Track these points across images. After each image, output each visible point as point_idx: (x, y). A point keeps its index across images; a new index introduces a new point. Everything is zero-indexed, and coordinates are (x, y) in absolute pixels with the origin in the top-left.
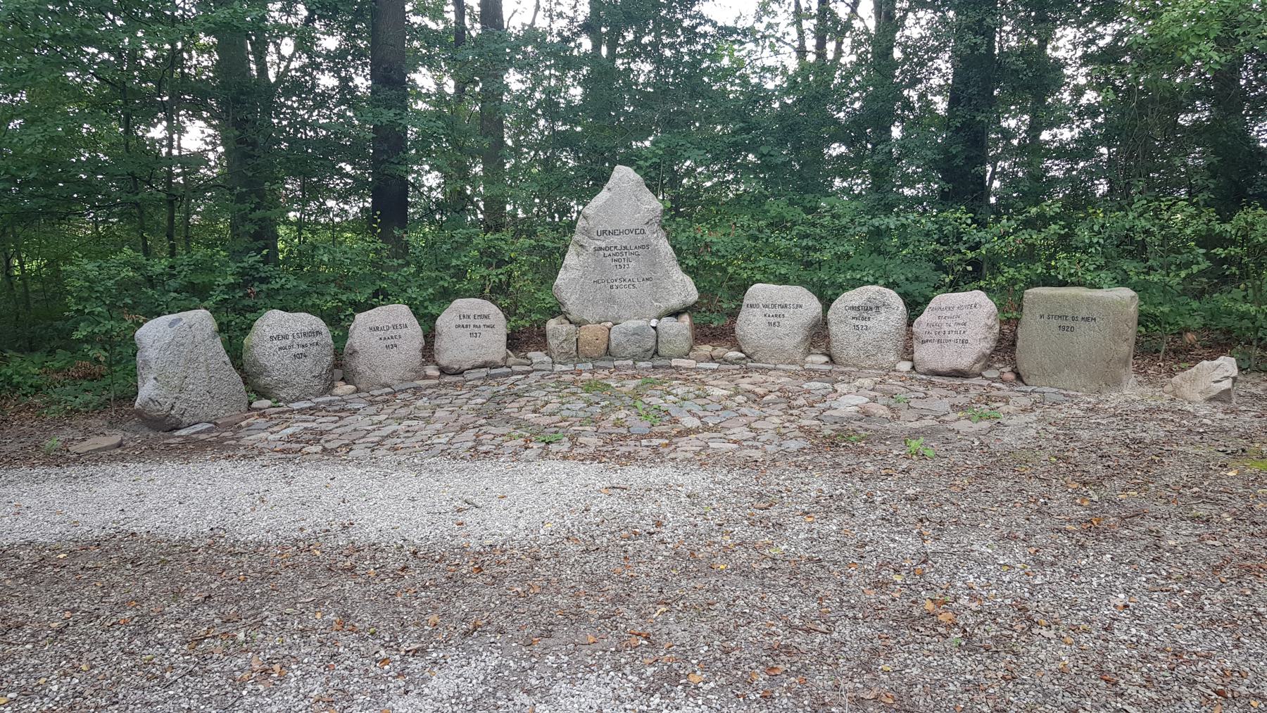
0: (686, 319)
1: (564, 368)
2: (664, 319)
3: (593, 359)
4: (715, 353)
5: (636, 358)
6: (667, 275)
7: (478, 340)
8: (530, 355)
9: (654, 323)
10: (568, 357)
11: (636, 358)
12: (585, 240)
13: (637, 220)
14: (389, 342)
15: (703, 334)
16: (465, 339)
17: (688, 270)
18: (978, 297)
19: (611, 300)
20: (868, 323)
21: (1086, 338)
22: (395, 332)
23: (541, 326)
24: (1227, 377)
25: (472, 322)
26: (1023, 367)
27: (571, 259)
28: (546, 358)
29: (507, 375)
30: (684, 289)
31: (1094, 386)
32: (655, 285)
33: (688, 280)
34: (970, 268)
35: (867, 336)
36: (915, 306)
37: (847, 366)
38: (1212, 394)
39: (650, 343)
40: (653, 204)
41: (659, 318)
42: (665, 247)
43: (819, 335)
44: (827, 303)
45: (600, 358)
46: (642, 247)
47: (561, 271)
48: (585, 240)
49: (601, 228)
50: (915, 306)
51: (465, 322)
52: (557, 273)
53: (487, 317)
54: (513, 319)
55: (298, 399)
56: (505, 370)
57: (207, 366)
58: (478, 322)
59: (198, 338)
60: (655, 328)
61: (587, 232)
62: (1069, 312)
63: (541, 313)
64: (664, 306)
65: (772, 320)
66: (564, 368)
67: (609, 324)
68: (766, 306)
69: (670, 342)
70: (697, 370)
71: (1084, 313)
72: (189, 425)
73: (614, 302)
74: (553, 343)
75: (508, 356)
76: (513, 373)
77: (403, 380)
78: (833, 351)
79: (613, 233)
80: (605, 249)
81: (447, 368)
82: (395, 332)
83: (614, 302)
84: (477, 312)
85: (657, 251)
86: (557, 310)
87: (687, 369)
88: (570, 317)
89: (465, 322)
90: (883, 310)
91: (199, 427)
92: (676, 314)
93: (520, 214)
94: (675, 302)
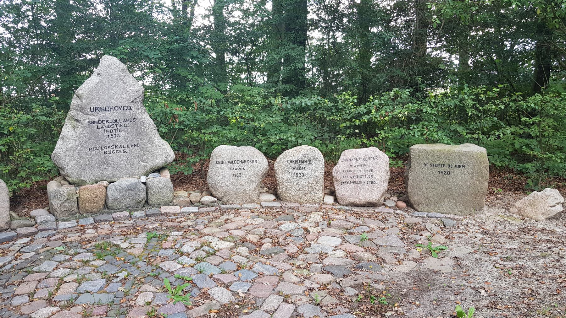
0: (167, 174)
1: (68, 225)
2: (151, 176)
3: (93, 213)
5: (131, 209)
8: (34, 213)
9: (143, 179)
10: (71, 215)
12: (80, 116)
15: (179, 181)
17: (164, 136)
18: (373, 151)
19: (106, 163)
20: (304, 172)
21: (458, 178)
23: (43, 188)
24: (558, 203)
26: (414, 197)
27: (67, 130)
28: (50, 217)
30: (164, 152)
31: (467, 211)
32: (142, 149)
33: (166, 143)
34: (357, 131)
35: (304, 181)
36: (331, 159)
37: (290, 202)
38: (551, 215)
39: (142, 196)
41: (147, 175)
43: (270, 183)
44: (272, 157)
45: (99, 212)
46: (130, 120)
47: (59, 142)
48: (80, 116)
49: (93, 106)
50: (331, 159)
52: (55, 143)
54: (14, 182)
60: (145, 184)
61: (81, 109)
62: (446, 162)
63: (41, 176)
64: (149, 165)
65: (236, 172)
66: (68, 225)
67: (105, 183)
68: (230, 162)
70: (182, 214)
71: (457, 162)
73: (108, 165)
74: (56, 203)
75: (12, 218)
76: (19, 236)
78: (280, 192)
79: (105, 109)
82: (241, 165)
83: (108, 165)
85: (142, 123)
86: (57, 172)
87: (174, 214)
88: (70, 180)
90: (313, 162)
92: (159, 170)
93: (14, 94)
94: (158, 162)
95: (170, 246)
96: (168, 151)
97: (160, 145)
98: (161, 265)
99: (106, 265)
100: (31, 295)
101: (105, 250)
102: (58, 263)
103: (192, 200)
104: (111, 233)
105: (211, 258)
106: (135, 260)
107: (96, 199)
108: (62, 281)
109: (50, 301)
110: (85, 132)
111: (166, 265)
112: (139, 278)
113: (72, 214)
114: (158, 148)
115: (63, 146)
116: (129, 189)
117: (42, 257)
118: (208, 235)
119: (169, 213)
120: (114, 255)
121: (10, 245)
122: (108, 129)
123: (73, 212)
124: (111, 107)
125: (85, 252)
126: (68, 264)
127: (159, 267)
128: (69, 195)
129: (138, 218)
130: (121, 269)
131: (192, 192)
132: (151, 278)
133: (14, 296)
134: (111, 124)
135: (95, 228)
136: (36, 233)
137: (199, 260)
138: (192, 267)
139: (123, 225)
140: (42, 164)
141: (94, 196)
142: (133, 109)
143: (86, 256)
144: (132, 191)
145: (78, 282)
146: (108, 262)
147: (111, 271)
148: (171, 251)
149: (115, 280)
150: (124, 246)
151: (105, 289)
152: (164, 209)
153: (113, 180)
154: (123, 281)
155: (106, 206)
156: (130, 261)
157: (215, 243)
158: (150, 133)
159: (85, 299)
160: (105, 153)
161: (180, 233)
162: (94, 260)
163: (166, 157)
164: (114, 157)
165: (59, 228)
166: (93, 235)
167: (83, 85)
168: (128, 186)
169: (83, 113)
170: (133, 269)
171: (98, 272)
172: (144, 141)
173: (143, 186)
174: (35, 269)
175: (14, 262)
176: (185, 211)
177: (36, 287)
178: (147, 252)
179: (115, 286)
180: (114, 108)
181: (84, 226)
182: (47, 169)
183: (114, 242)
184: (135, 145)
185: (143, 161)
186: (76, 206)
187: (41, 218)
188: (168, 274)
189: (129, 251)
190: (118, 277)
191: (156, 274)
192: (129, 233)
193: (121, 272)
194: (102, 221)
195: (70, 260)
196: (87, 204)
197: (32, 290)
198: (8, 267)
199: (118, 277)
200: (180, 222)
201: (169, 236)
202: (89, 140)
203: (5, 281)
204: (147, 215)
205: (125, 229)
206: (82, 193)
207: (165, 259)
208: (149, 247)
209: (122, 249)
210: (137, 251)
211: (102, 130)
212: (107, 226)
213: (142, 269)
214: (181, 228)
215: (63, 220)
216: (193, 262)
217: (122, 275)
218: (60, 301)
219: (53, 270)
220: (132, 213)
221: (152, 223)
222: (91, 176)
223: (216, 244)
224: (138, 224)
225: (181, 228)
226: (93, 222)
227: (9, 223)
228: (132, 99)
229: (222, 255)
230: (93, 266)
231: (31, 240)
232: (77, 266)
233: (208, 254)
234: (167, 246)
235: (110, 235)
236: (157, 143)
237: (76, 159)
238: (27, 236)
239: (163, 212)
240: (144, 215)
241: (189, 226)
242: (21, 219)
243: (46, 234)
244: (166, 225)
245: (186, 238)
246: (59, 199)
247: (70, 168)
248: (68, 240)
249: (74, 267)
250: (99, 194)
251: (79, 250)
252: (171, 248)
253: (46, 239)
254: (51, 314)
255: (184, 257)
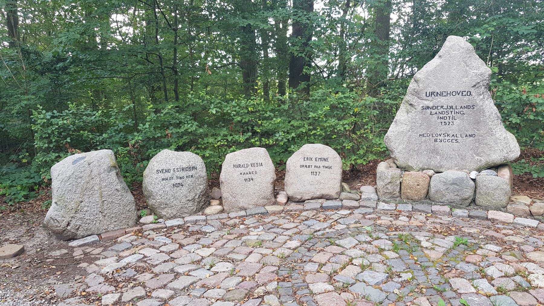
0: (506, 173)
2: (484, 172)
3: (413, 201)
4: (535, 209)
5: (453, 205)
6: (490, 133)
7: (317, 178)
9: (473, 175)
11: (453, 205)
12: (414, 100)
13: (464, 84)
14: (247, 176)
16: (306, 175)
17: (511, 127)
19: (435, 151)
22: (252, 169)
25: (313, 163)
27: (401, 115)
29: (337, 208)
30: (508, 146)
39: (469, 193)
40: (483, 69)
41: (479, 170)
42: (489, 106)
45: (419, 201)
46: (468, 107)
47: (393, 126)
48: (414, 100)
49: (430, 90)
51: (308, 163)
53: (326, 160)
55: (174, 217)
56: (337, 203)
57: (101, 193)
58: (319, 163)
59: (95, 172)
60: (474, 180)
61: (416, 93)
64: (484, 160)
67: (431, 172)
69: (487, 194)
70: (514, 227)
72: (83, 237)
73: (437, 153)
76: (342, 207)
77: (257, 205)
79: (441, 94)
80: (432, 108)
81: (292, 197)
82: (252, 169)
84: (319, 156)
85: (482, 111)
86: (386, 154)
87: (504, 223)
88: (397, 163)
89: (308, 163)
91: (90, 239)
92: (496, 167)
94: (496, 157)
95: (475, 261)
96: (512, 146)
97: (502, 138)
98: (452, 281)
99: (396, 260)
100: (321, 265)
101: (405, 244)
102: (357, 242)
103: (532, 211)
104: (421, 226)
105: (520, 294)
106: (426, 264)
107: (418, 187)
108: (351, 262)
109: (331, 278)
110: (417, 117)
111: (459, 283)
112: (422, 286)
113: (394, 197)
114: (499, 141)
115: (394, 130)
116: (454, 183)
117: (349, 232)
118: (533, 262)
119: (497, 220)
120: (411, 251)
121: (333, 213)
122: (441, 116)
123: (394, 196)
124: (449, 92)
125: (386, 239)
126: (365, 246)
127: (449, 283)
128: (393, 178)
129: (459, 217)
130: (409, 269)
131: (537, 201)
132: (434, 292)
133: (310, 261)
134: (445, 110)
135: (410, 217)
136: (357, 208)
137: (501, 291)
138: (488, 296)
139: (439, 221)
140: (380, 144)
141: (416, 184)
142: (473, 94)
143: (384, 243)
144: (458, 185)
145: (363, 267)
146: (400, 257)
147: (398, 267)
148: (472, 268)
149: (396, 279)
150: (424, 244)
151: (381, 286)
152: (492, 214)
153: (441, 170)
154: (403, 284)
155: (427, 195)
156: (422, 264)
157: (536, 275)
158: (490, 123)
159: (358, 288)
160: (436, 141)
161: (497, 248)
162: (389, 250)
163: (507, 153)
164: (444, 147)
165: (378, 208)
166: (403, 223)
167: (422, 69)
168: (453, 179)
169: (418, 98)
170: (421, 273)
171: (385, 264)
172: (482, 131)
173: (472, 183)
174: (337, 242)
175: (327, 230)
176: (519, 222)
177: (329, 260)
178: (445, 259)
179: (393, 287)
180: (451, 94)
181: (401, 211)
182: (382, 150)
183: (417, 237)
184: (470, 136)
185: (478, 155)
186: (398, 190)
187: (365, 195)
188: (454, 295)
189: (426, 252)
190: (401, 277)
191: (440, 289)
192: (440, 231)
193: (406, 272)
194: (419, 211)
195: (370, 243)
196: (409, 191)
197: (323, 262)
198: (319, 233)
199: (401, 277)
200: (506, 235)
201: (481, 248)
202: (420, 126)
203: (311, 244)
204: (469, 216)
205: (438, 226)
206: (405, 178)
207: (461, 275)
208: (451, 255)
209: (422, 247)
210: (433, 255)
211: (435, 116)
212: (422, 218)
213: (430, 277)
214: (502, 243)
215: (384, 201)
216: (493, 291)
217: (406, 276)
218: (338, 282)
219: (350, 248)
220: (453, 209)
221: (472, 227)
222: (418, 163)
223: (537, 278)
224: (455, 224)
225: (502, 243)
226: (411, 210)
227: (339, 194)
228: (474, 83)
229: (538, 296)
230: (385, 256)
231: (350, 214)
232: (371, 251)
233: (519, 288)
234: (471, 260)
235: (419, 228)
236: (497, 136)
237: (405, 143)
238: (349, 208)
239: (489, 217)
240: (466, 215)
241: (514, 243)
242: (352, 192)
243: (364, 210)
244: (487, 233)
245: (501, 257)
246: (383, 180)
247: (398, 152)
248: (379, 222)
249: (368, 251)
250: (421, 183)
251: (381, 235)
252: (475, 264)
253: (361, 216)
254: (323, 291)
255: (485, 280)
